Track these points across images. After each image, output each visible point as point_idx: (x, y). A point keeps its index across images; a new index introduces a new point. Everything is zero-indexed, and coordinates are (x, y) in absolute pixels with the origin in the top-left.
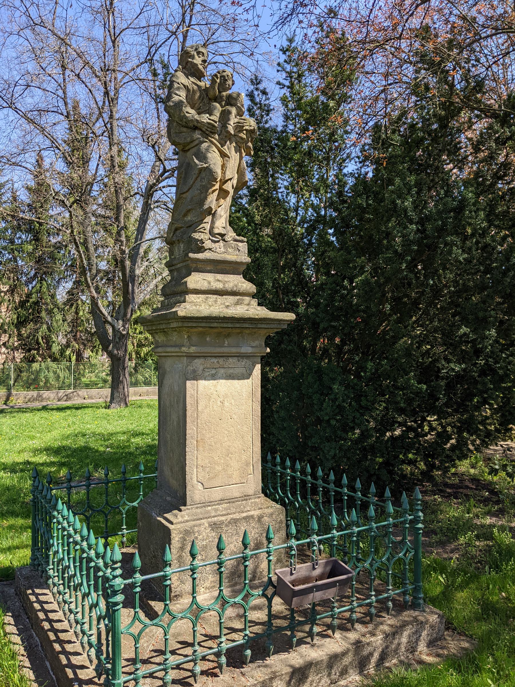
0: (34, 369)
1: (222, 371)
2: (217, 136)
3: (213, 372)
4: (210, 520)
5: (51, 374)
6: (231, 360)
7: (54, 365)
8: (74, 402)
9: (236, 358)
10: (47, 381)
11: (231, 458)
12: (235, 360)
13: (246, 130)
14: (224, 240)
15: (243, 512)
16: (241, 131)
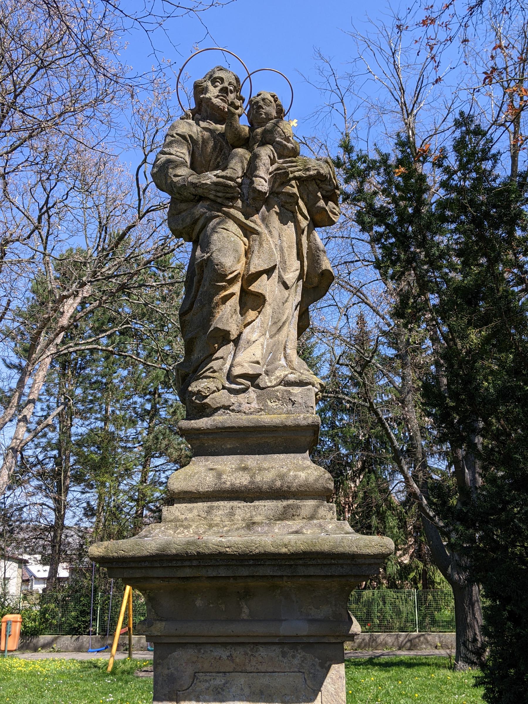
0: (365, 598)
1: (241, 680)
2: (239, 203)
3: (219, 681)
5: (388, 607)
6: (263, 652)
7: (391, 594)
8: (420, 653)
9: (277, 650)
10: (382, 619)
12: (274, 652)
13: (295, 178)
14: (258, 387)
16: (286, 182)
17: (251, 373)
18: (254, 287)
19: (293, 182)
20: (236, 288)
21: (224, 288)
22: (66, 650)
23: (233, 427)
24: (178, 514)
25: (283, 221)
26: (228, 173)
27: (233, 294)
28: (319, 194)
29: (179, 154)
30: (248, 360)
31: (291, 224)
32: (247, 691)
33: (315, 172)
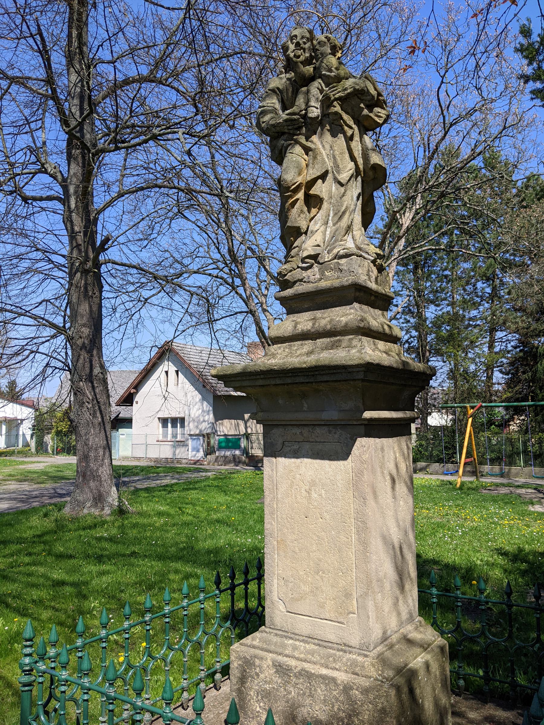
1: (307, 446)
3: (296, 447)
4: (280, 658)
6: (318, 430)
9: (326, 428)
11: (322, 578)
13: (336, 99)
14: (319, 263)
15: (327, 667)
16: (331, 105)
17: (312, 254)
18: (313, 191)
19: (335, 103)
20: (301, 195)
21: (291, 197)
22: (437, 473)
23: (304, 293)
24: (273, 350)
25: (334, 135)
26: (295, 109)
27: (298, 199)
28: (362, 105)
29: (269, 105)
30: (312, 245)
31: (341, 136)
32: (310, 453)
33: (352, 89)
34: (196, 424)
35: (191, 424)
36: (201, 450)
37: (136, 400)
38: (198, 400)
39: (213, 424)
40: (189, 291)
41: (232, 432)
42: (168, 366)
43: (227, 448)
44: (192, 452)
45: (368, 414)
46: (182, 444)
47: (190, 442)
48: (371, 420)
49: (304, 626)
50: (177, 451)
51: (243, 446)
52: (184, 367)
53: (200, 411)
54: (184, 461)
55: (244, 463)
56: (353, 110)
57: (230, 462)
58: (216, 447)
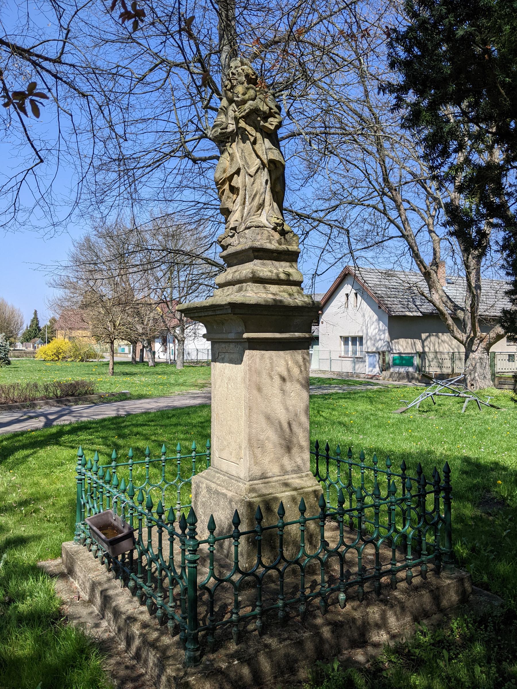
20: (226, 186)
25: (244, 142)
28: (259, 119)
34: (373, 342)
35: (369, 342)
36: (377, 366)
37: (321, 320)
38: (374, 320)
39: (388, 342)
40: (329, 225)
41: (409, 350)
42: (347, 288)
43: (401, 365)
44: (369, 368)
45: (246, 335)
46: (361, 360)
47: (367, 358)
48: (248, 339)
49: (224, 468)
50: (357, 367)
51: (415, 363)
52: (362, 290)
53: (377, 330)
54: (362, 376)
55: (417, 379)
56: (254, 122)
57: (403, 378)
58: (391, 364)
